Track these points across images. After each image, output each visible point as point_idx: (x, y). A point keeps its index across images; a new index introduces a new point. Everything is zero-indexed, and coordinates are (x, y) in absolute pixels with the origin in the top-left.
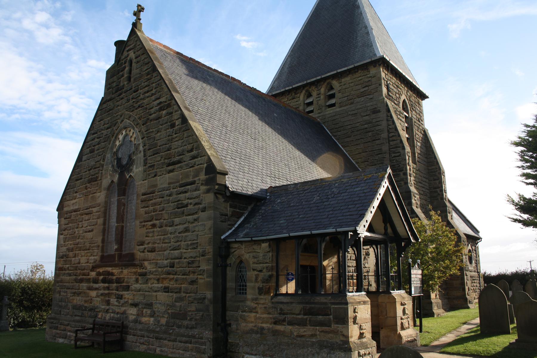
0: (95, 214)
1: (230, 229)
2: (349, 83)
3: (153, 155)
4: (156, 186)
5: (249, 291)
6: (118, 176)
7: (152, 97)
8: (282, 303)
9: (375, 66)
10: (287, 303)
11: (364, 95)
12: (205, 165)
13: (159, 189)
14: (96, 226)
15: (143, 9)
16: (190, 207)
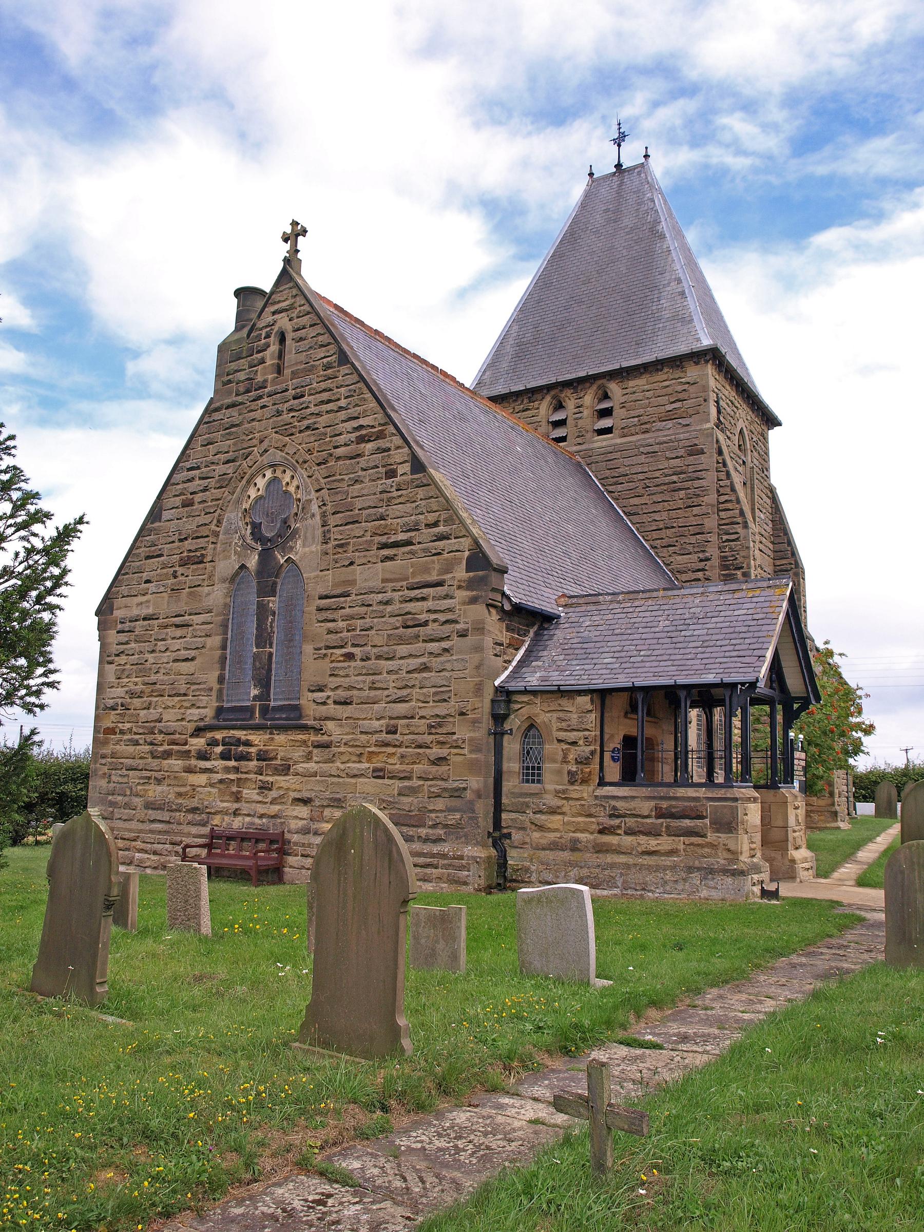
0: (198, 627)
1: (506, 668)
2: (644, 391)
3: (346, 525)
4: (353, 582)
5: (547, 776)
6: (257, 557)
7: (339, 414)
8: (614, 798)
9: (697, 363)
10: (625, 797)
11: (673, 417)
12: (467, 553)
13: (360, 588)
14: (203, 650)
15: (304, 232)
16: (432, 626)
